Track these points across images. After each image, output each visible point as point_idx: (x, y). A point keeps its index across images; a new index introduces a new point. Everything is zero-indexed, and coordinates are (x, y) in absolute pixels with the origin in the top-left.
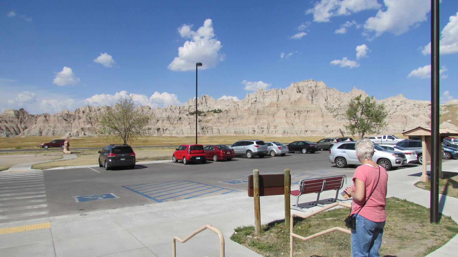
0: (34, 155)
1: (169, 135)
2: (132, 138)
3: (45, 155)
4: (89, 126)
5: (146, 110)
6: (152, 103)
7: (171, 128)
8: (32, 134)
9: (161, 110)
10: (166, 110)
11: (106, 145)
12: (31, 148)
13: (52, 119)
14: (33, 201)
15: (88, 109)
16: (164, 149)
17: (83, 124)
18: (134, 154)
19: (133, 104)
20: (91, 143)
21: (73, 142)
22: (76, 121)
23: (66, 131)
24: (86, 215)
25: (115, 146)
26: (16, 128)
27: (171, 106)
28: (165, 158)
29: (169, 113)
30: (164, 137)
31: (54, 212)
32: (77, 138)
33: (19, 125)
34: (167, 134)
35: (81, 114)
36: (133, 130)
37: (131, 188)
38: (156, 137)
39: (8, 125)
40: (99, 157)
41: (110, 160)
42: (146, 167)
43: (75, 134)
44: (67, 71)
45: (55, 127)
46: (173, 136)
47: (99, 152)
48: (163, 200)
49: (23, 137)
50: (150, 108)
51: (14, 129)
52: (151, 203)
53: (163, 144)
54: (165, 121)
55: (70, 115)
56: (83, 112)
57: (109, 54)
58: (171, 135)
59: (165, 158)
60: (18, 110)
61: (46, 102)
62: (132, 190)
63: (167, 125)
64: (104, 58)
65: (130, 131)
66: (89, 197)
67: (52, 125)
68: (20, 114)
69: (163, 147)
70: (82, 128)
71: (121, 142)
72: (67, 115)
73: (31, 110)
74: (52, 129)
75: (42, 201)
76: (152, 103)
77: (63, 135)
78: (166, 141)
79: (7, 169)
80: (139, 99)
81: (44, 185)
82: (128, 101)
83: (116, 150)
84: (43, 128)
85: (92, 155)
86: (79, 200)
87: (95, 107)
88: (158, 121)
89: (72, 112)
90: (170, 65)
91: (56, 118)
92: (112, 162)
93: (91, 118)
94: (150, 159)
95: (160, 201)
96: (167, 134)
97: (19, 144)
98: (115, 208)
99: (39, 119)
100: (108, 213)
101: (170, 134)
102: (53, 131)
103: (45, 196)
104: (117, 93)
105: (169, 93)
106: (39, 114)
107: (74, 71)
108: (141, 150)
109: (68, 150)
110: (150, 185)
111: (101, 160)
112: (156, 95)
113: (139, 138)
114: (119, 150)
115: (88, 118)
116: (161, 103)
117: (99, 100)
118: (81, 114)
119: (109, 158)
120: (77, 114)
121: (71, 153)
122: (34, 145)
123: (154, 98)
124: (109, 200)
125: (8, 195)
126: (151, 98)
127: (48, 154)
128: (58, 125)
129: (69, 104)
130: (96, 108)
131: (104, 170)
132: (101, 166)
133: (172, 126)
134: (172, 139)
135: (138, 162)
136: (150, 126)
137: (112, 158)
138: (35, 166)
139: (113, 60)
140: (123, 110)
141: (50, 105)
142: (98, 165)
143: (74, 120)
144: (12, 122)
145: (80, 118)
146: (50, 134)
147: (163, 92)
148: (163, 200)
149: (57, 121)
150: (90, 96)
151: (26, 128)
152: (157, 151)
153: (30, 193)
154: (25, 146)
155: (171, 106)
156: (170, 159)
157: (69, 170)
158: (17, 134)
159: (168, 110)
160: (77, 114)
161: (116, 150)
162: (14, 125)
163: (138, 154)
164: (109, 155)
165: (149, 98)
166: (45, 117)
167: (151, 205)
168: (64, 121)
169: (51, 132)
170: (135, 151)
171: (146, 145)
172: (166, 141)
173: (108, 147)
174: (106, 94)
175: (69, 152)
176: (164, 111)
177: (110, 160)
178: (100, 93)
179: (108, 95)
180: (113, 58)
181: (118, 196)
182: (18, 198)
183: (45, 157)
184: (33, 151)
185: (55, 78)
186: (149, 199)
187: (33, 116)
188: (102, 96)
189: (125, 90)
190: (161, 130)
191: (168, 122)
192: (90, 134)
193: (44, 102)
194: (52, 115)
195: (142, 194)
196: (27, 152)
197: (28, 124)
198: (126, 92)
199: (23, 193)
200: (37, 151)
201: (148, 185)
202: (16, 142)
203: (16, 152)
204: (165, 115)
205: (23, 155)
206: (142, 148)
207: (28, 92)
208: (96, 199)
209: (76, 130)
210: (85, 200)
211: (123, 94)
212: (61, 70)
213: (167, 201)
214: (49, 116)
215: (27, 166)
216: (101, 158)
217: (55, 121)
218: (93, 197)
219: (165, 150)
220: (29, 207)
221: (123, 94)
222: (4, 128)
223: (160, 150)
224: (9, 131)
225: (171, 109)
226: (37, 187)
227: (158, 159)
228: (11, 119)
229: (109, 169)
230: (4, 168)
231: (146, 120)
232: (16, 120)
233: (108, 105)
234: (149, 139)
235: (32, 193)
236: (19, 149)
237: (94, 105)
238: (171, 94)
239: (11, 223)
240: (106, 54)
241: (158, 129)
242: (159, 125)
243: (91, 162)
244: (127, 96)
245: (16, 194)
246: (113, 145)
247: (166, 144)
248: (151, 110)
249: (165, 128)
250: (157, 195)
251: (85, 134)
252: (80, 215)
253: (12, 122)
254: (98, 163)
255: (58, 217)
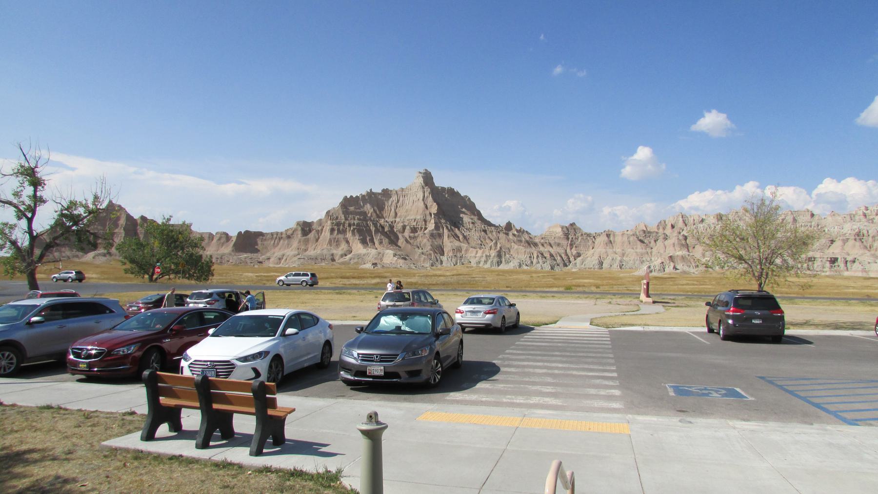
0: (592, 302)
1: (860, 274)
2: (776, 278)
3: (610, 303)
4: (684, 252)
5: (803, 219)
6: (817, 202)
7: (866, 257)
8: (587, 266)
9: (839, 219)
10: (852, 217)
11: (722, 291)
12: (586, 290)
13: (618, 239)
14: (598, 381)
15: (681, 219)
16: (849, 305)
17: (672, 248)
18: (782, 312)
19: (777, 208)
20: (687, 284)
21: (655, 282)
22: (660, 242)
23: (642, 262)
24: (691, 422)
25: (740, 293)
26: (563, 256)
27: (867, 209)
28: (853, 326)
29: (861, 225)
30: (847, 278)
31: (633, 407)
32: (660, 275)
33: (568, 250)
34: (855, 271)
35: (668, 231)
36: (778, 261)
37: (779, 383)
38: (828, 276)
39: (552, 251)
40: (706, 313)
41: (730, 322)
42: (810, 343)
43: (657, 268)
44: (643, 153)
45: (623, 255)
46: (872, 275)
47: (708, 304)
48: (861, 420)
49: (574, 270)
50: (812, 215)
51: (561, 256)
52: (828, 424)
53: (846, 294)
54: (851, 242)
55: (649, 232)
56: (673, 227)
57: (720, 110)
58: (865, 275)
59: (853, 326)
60: (567, 225)
61: (610, 210)
62: (781, 387)
63: (854, 250)
64: (712, 121)
65: (771, 263)
66: (693, 389)
67: (619, 250)
68: (571, 232)
69: (847, 299)
70: (671, 257)
71: (753, 287)
72: (644, 232)
73: (586, 226)
74: (619, 258)
75: (611, 383)
76: (817, 202)
77: (636, 269)
78: (854, 288)
79: (555, 322)
80: (788, 197)
81: (611, 356)
82: (767, 203)
83: (741, 302)
84: (605, 256)
85: (692, 309)
86: (675, 392)
87: (694, 215)
88: (832, 241)
89: (653, 227)
90: (863, 115)
91: (625, 238)
92: (734, 325)
93: (686, 238)
94: (816, 326)
95: (853, 422)
96: (855, 271)
97: (569, 282)
98: (748, 420)
99: (598, 240)
100: (734, 428)
101: (864, 270)
102: (621, 262)
103: (615, 375)
104: (738, 188)
105: (859, 178)
106: (598, 232)
107: (655, 152)
108: (793, 303)
109: (648, 296)
110: (819, 381)
111: (711, 320)
112: (828, 186)
113: (789, 279)
114: (749, 303)
115: (681, 237)
116: (841, 202)
117: (703, 203)
118: (668, 231)
119: (728, 317)
120: (661, 231)
121: (654, 302)
122: (591, 285)
123: (823, 191)
124: (734, 401)
125: (560, 365)
126: (815, 192)
127: (614, 301)
128: (629, 250)
129: (646, 212)
130: (696, 218)
131: (716, 340)
132: (711, 331)
133: (868, 254)
134: (868, 283)
135: (789, 328)
136: (810, 254)
137: (733, 317)
138: (596, 321)
139: (729, 122)
140: (756, 221)
141: (615, 215)
142: (706, 330)
143: (655, 241)
144: (559, 245)
145: (666, 238)
146: (616, 266)
147: (844, 178)
148: (861, 420)
149: (627, 243)
150: (684, 197)
151: (579, 255)
152: (832, 307)
153: (591, 367)
154: (579, 286)
155: (867, 209)
156: (868, 330)
157: (632, 332)
158: (565, 265)
159: (857, 218)
160: (661, 231)
161: (741, 302)
162: (562, 251)
163: (791, 312)
164: (729, 311)
165: (809, 194)
166: (608, 236)
167: (829, 427)
168: (639, 243)
169: (618, 262)
170: (783, 305)
171: (807, 294)
172: (854, 288)
173: (726, 294)
174: (715, 189)
175: (650, 300)
176: (848, 218)
177: (730, 322)
178: (701, 190)
179: (719, 192)
180: (729, 118)
181: (752, 395)
182: (574, 373)
183: (610, 306)
184: (591, 296)
185: (624, 167)
186: (823, 414)
187: (589, 235)
188: (708, 194)
189: (753, 180)
190: (841, 263)
191: (858, 244)
192: (686, 268)
193: (606, 210)
194: (618, 232)
195: (804, 399)
196: (581, 296)
197: (582, 250)
198: (757, 184)
199: (581, 366)
200: (598, 296)
201: (819, 381)
202: (564, 279)
203: (566, 295)
204: (849, 228)
205: (576, 301)
206: (796, 300)
207: (581, 196)
208: (707, 395)
209: (660, 261)
210: (688, 393)
211: (751, 188)
212: (634, 152)
213: (871, 425)
214: (614, 235)
215: (584, 320)
216: (710, 315)
217: (623, 243)
218: (701, 390)
219: (853, 308)
220: (592, 391)
221: (751, 188)
222: (547, 255)
223: (840, 306)
224: (555, 260)
225: (865, 215)
226: (603, 358)
227: (837, 327)
228: (557, 241)
229: (726, 338)
230: (550, 319)
231: (800, 243)
232: (564, 242)
233: (718, 212)
234: (815, 280)
235: (596, 367)
236: (569, 290)
237: (693, 212)
238: (867, 180)
239: (568, 413)
240: (714, 112)
241: (833, 261)
242: (835, 250)
243: (691, 321)
244: (759, 191)
245: (572, 366)
246: (737, 291)
247: (853, 293)
248: (816, 218)
249: (849, 258)
250: (842, 407)
251: (675, 268)
252: (680, 421)
253: (559, 245)
254: (705, 324)
255: (640, 418)
